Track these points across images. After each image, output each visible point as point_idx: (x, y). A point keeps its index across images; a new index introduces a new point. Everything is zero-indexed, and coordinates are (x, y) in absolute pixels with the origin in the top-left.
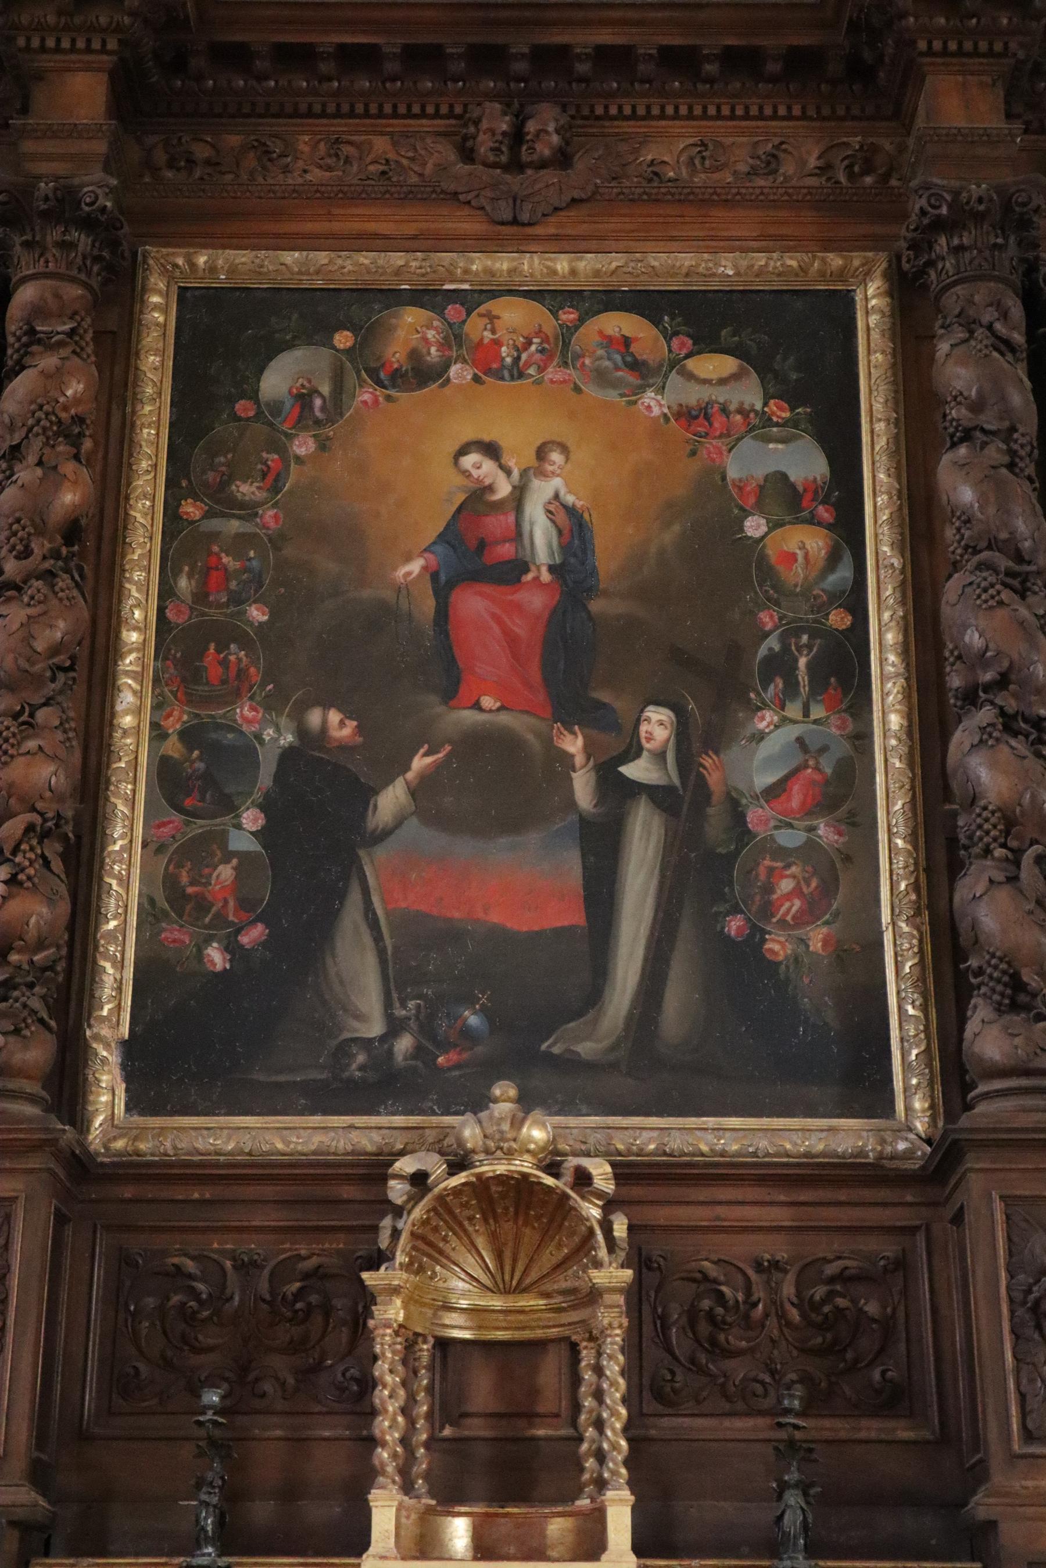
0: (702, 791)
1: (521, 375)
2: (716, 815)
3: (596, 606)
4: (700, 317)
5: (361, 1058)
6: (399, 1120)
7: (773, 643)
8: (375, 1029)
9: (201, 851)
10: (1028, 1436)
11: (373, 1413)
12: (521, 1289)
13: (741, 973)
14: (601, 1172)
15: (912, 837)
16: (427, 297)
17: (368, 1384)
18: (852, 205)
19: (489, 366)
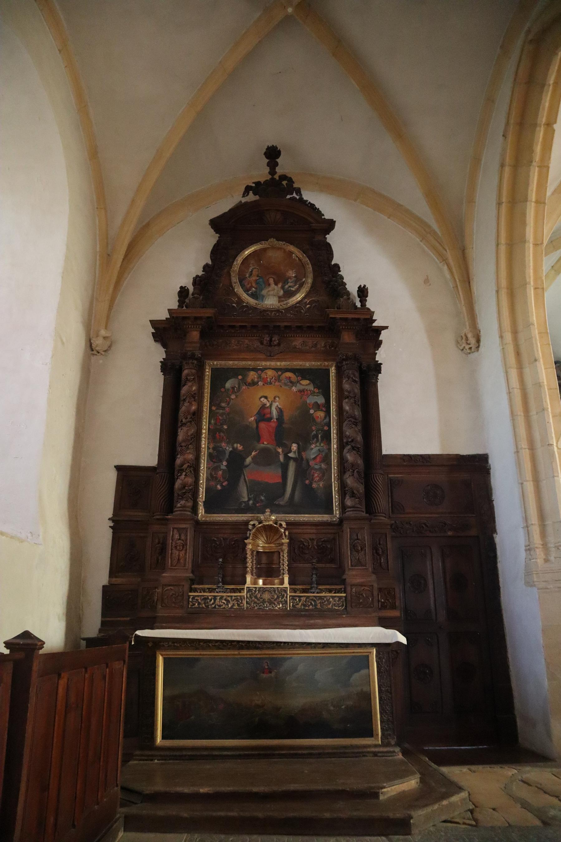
0: (302, 459)
1: (271, 384)
2: (304, 462)
3: (284, 426)
4: (302, 373)
5: (244, 504)
6: (250, 515)
7: (315, 432)
8: (246, 499)
9: (216, 469)
10: (352, 566)
11: (246, 563)
12: (270, 543)
13: (308, 490)
14: (284, 524)
15: (338, 467)
16: (254, 369)
17: (246, 558)
18: (330, 353)
19: (266, 382)
